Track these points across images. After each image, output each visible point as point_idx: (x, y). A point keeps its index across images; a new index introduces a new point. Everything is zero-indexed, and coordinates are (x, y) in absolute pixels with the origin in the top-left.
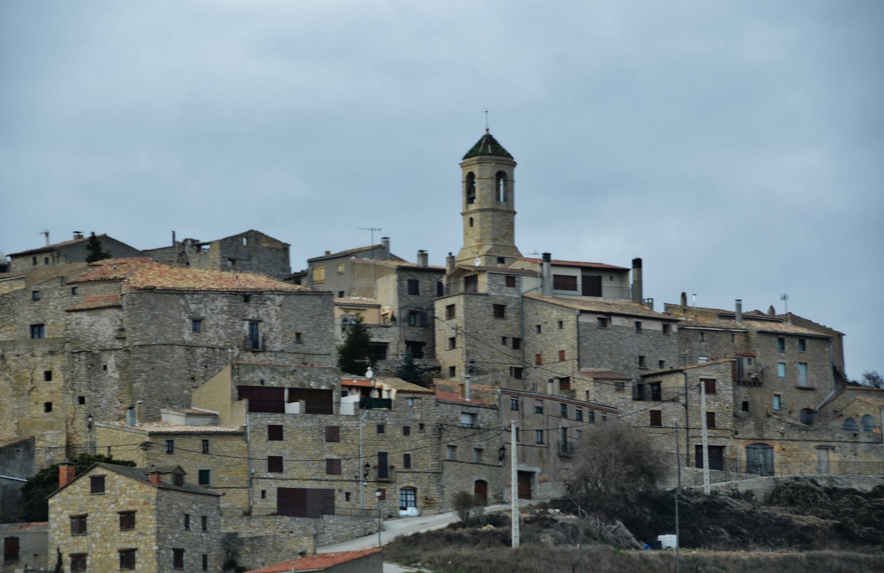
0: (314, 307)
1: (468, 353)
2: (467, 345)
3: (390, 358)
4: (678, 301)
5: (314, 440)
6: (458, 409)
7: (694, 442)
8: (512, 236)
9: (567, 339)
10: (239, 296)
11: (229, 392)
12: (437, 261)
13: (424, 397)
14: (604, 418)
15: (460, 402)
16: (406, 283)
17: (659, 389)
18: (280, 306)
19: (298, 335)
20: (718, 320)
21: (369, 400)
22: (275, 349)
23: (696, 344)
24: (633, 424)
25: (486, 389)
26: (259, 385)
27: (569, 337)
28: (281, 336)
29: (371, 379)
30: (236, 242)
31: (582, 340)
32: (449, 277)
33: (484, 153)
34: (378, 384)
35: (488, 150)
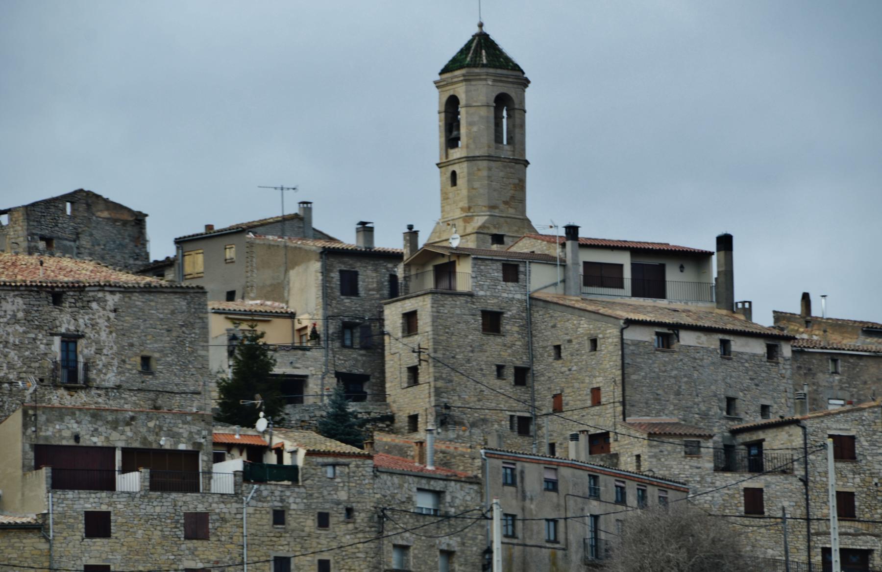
0: (173, 313)
1: (438, 392)
2: (436, 379)
3: (309, 400)
4: (796, 308)
5: (164, 537)
6: (412, 484)
7: (819, 543)
8: (523, 201)
9: (605, 369)
10: (43, 295)
11: (20, 455)
12: (389, 239)
13: (353, 462)
14: (663, 500)
15: (415, 471)
16: (335, 276)
17: (760, 453)
18: (115, 311)
19: (146, 361)
20: (862, 338)
21: (259, 468)
22: (107, 384)
23: (823, 378)
24: (715, 511)
25: (461, 449)
26: (72, 443)
27: (607, 365)
28: (115, 362)
29: (265, 432)
30: (53, 210)
31: (629, 370)
32: (408, 266)
33: (474, 64)
34: (277, 441)
35: (482, 55)
